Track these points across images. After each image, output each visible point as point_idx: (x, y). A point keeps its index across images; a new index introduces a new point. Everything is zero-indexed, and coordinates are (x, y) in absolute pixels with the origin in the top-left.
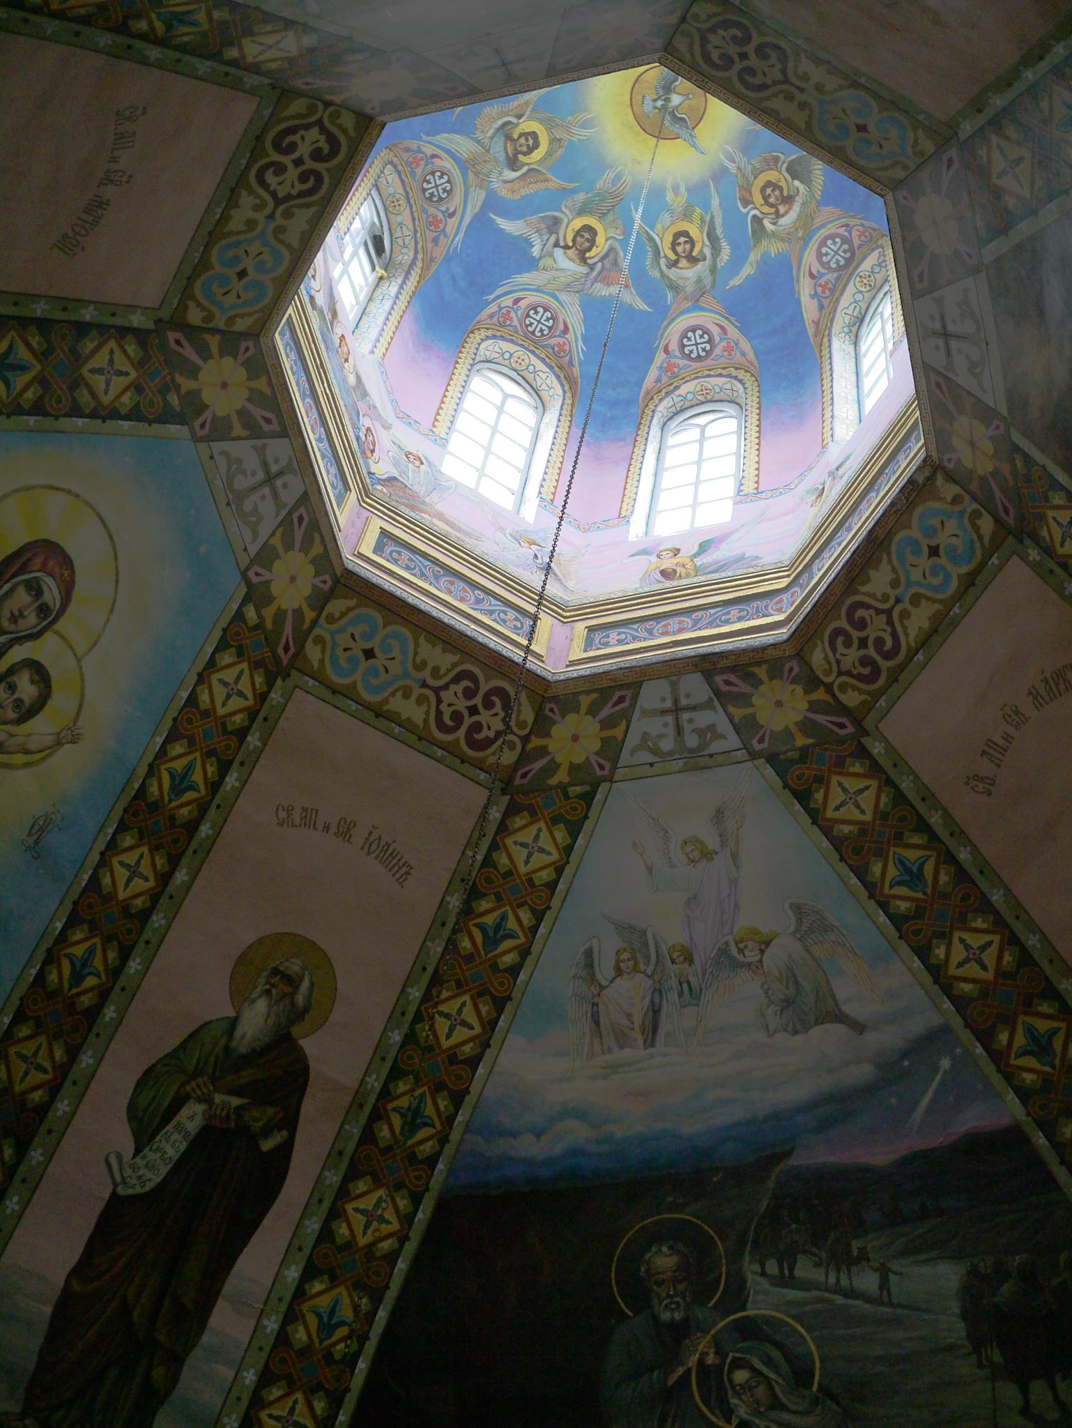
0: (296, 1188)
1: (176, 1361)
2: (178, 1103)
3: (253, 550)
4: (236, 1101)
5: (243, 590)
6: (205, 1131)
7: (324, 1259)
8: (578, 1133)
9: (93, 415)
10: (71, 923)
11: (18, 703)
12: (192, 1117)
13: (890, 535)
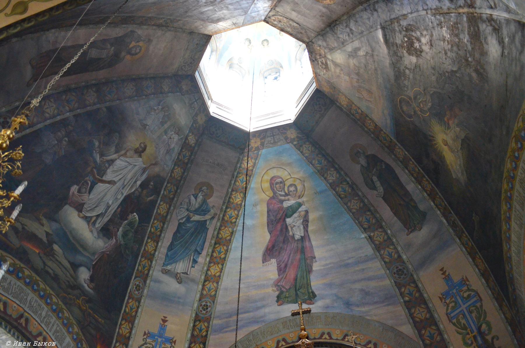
0: (393, 164)
1: (412, 200)
2: (372, 180)
3: (284, 140)
4: (375, 170)
5: (290, 144)
6: (378, 177)
7: (405, 164)
8: (386, 112)
9: (254, 167)
10: (334, 190)
11: (294, 191)
12: (375, 179)
13: (279, 27)
